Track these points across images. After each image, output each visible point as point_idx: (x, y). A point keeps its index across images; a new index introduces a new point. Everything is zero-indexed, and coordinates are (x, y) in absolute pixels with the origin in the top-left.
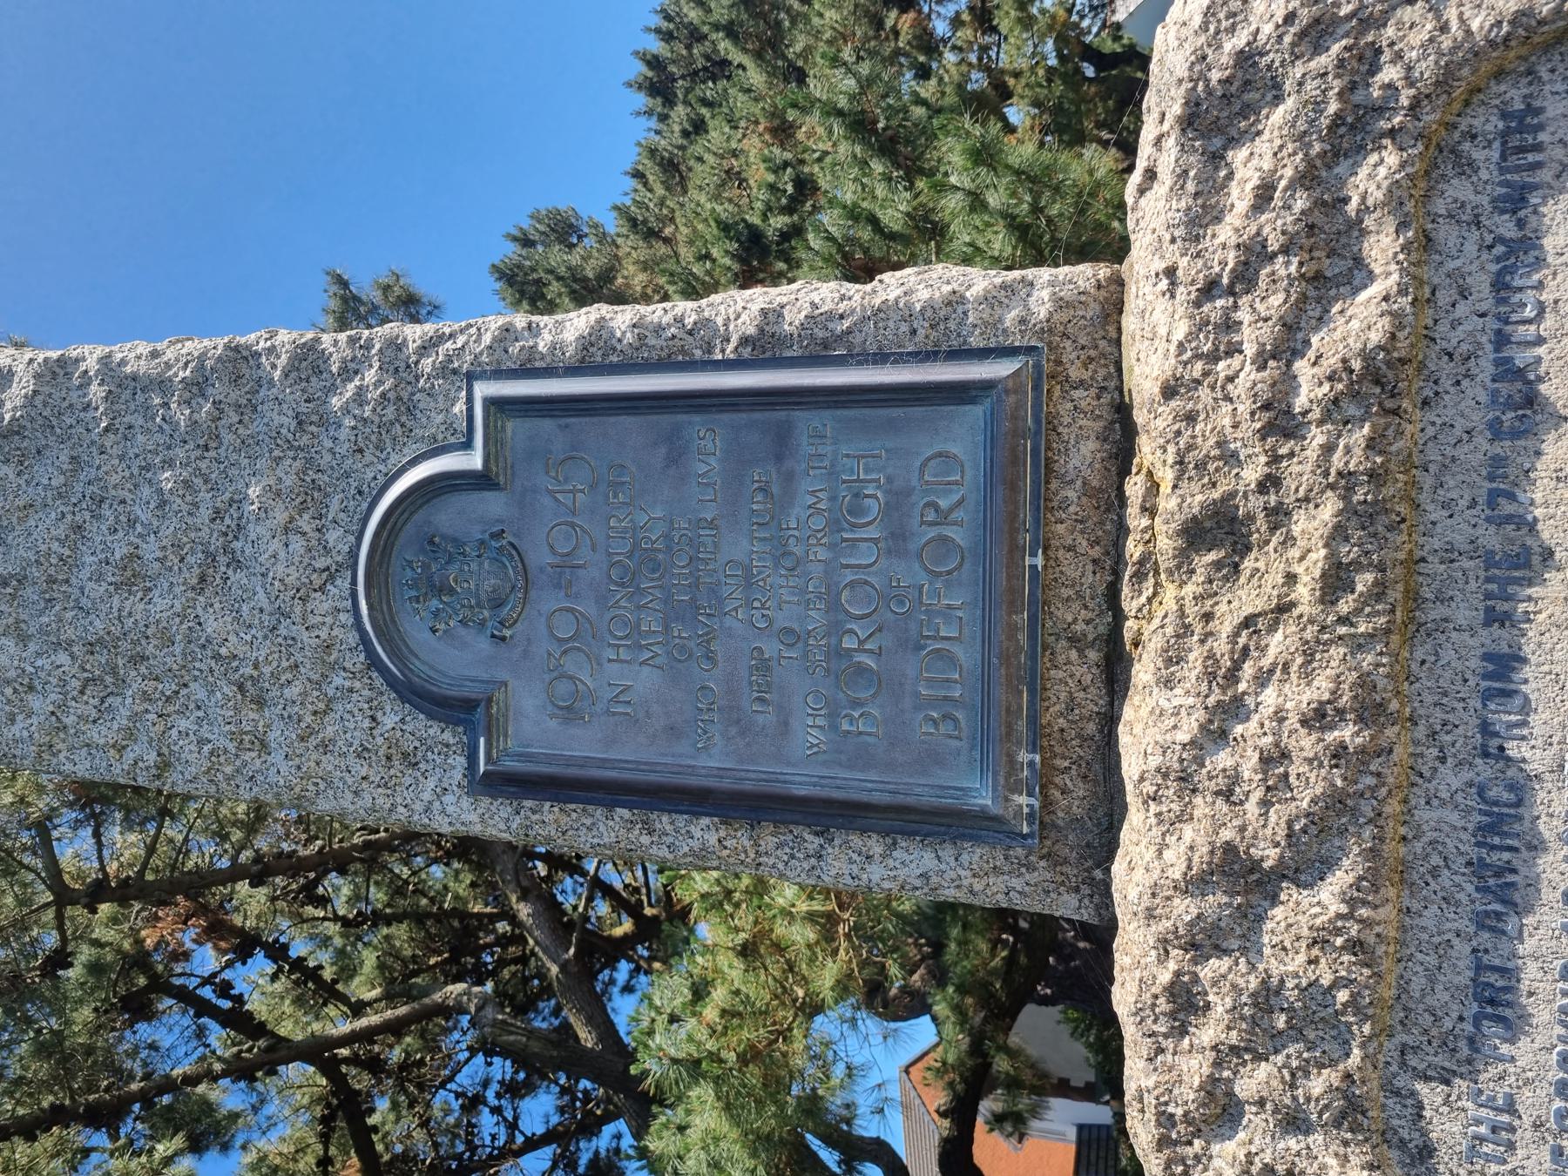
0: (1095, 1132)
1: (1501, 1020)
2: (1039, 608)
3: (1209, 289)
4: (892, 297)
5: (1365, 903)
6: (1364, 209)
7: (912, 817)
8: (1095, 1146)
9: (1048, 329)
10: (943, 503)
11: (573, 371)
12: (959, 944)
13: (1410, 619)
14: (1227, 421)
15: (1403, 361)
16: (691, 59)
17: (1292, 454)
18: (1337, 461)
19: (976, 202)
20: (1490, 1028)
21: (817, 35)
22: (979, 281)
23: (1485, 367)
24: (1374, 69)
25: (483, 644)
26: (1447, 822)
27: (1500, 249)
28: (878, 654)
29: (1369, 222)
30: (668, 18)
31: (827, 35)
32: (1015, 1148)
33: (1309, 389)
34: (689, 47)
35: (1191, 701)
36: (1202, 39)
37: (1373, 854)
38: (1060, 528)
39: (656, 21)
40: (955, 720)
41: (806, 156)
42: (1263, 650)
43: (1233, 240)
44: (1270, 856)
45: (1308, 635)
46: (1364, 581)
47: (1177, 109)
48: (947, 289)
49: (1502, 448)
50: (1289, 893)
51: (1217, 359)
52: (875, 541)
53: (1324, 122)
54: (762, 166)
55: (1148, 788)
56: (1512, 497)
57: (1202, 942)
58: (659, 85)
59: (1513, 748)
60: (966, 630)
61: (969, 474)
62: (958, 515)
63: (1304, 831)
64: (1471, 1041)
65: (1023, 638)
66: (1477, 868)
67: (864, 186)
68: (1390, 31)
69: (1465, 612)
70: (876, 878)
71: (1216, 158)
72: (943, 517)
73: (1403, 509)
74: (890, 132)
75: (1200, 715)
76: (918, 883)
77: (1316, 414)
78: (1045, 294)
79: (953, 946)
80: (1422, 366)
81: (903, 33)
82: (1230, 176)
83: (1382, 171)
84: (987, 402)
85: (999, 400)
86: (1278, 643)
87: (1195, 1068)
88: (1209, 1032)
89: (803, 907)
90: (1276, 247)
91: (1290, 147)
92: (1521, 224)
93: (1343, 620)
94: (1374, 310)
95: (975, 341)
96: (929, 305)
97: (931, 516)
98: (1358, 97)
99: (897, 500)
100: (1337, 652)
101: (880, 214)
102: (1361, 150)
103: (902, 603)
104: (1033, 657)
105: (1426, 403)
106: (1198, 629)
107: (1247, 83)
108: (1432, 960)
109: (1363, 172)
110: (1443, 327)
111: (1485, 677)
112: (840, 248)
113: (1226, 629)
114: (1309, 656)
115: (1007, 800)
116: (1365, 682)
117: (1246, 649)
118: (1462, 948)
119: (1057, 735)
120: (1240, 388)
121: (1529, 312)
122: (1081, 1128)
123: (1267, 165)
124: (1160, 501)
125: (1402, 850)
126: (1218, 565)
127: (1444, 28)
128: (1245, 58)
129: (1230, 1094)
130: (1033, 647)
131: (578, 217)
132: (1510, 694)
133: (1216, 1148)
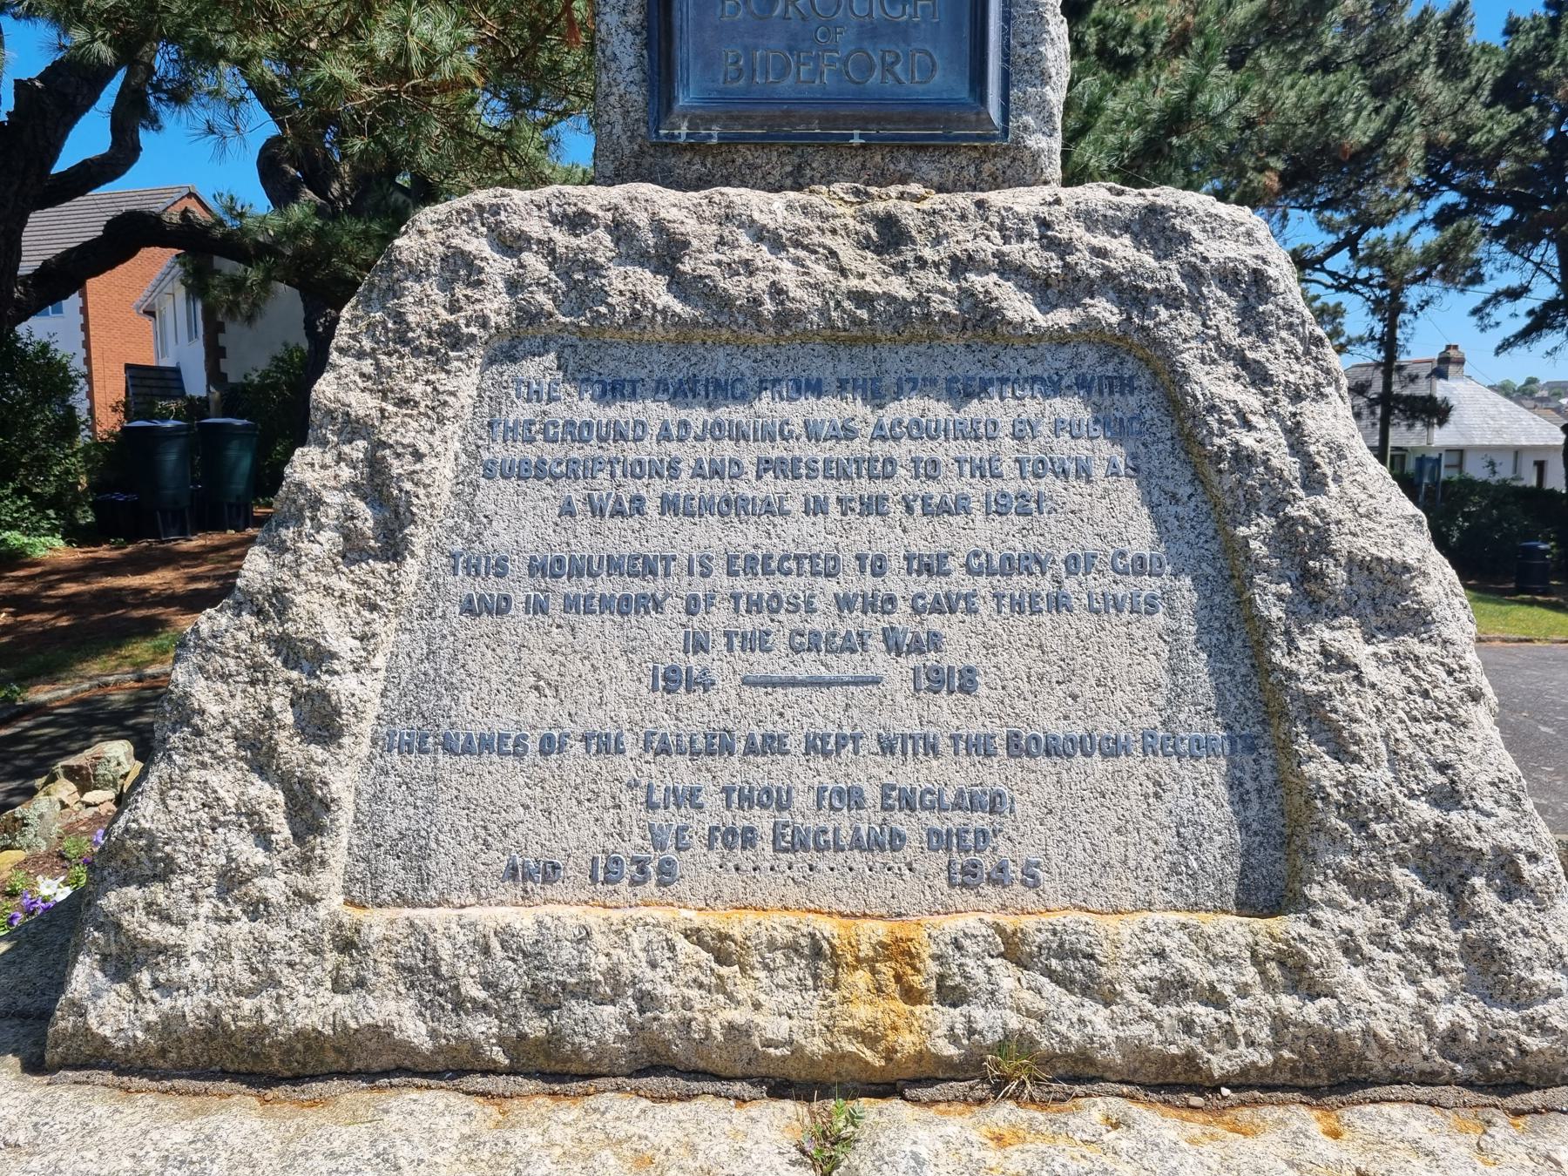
1: (604, 393)
3: (1044, 224)
4: (1050, 28)
5: (665, 319)
6: (1085, 307)
7: (663, 44)
8: (162, 383)
9: (1018, 145)
10: (898, 68)
12: (365, 232)
13: (840, 339)
14: (960, 238)
15: (994, 331)
17: (940, 273)
18: (936, 297)
20: (598, 388)
21: (1274, 83)
22: (1056, 96)
23: (988, 374)
24: (1167, 307)
26: (719, 363)
27: (1056, 378)
28: (784, 17)
29: (1078, 310)
31: (1272, 94)
32: (138, 308)
33: (976, 281)
35: (780, 220)
36: (1201, 213)
37: (695, 323)
38: (878, 158)
40: (738, 78)
41: (1155, 68)
42: (817, 261)
43: (1074, 236)
44: (686, 266)
45: (827, 286)
46: (863, 314)
47: (1159, 201)
48: (1053, 71)
49: (942, 384)
50: (662, 281)
51: (1000, 230)
52: (870, 14)
53: (1140, 283)
54: (1151, 19)
55: (717, 198)
56: (913, 389)
57: (621, 230)
59: (766, 395)
60: (805, 86)
61: (920, 88)
62: (890, 79)
63: (705, 285)
64: (588, 380)
65: (801, 129)
66: (694, 379)
67: (1118, 122)
68: (1188, 314)
69: (844, 370)
70: (607, 18)
71: (1126, 228)
72: (888, 68)
73: (907, 334)
74: (1166, 149)
75: (772, 226)
76: (608, 53)
77: (964, 284)
78: (1044, 145)
79: (360, 227)
80: (990, 343)
81: (1260, 177)
82: (1114, 236)
83: (1107, 315)
84: (970, 101)
85: (972, 108)
86: (821, 271)
87: (535, 227)
88: (561, 238)
89: (413, 43)
90: (1068, 259)
91: (1128, 265)
92: (1069, 387)
93: (838, 304)
94: (1026, 314)
95: (1014, 93)
96: (1042, 58)
97: (889, 59)
98: (1153, 299)
99: (901, 32)
100: (819, 302)
101: (1091, 137)
102: (1120, 303)
103: (824, 36)
104: (788, 136)
105: (968, 346)
106: (826, 226)
107: (1170, 240)
108: (632, 359)
109: (1108, 306)
110: (1012, 353)
111: (807, 380)
113: (828, 240)
114: (815, 286)
115: (684, 116)
116: (801, 316)
117: (816, 252)
118: (643, 374)
119: (730, 157)
120: (982, 242)
121: (1018, 393)
122: (176, 371)
123: (1118, 254)
124: (904, 203)
125: (697, 342)
126: (867, 237)
127: (1185, 341)
128: (1186, 238)
129: (521, 250)
130: (795, 137)
132: (799, 390)
133: (484, 241)
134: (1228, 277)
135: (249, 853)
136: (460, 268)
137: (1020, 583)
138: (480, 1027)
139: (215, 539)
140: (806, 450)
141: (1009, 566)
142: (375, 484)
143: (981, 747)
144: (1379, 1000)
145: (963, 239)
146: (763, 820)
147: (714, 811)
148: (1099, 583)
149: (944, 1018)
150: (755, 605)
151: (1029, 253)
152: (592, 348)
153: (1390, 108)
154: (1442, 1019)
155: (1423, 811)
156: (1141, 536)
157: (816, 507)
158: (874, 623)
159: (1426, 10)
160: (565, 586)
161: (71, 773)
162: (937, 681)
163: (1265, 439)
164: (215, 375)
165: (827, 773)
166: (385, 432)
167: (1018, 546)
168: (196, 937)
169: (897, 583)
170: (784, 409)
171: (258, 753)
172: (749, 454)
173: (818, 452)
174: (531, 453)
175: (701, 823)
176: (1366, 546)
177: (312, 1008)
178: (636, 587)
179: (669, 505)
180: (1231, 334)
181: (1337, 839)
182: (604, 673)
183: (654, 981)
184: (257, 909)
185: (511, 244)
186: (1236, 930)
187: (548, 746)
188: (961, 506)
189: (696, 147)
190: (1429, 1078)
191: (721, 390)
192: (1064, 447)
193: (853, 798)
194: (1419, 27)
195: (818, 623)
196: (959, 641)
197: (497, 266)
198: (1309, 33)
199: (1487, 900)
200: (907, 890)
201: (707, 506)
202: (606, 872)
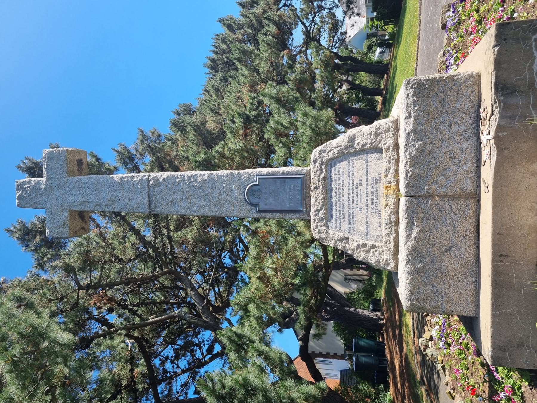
0: (345, 372)
2: (305, 194)
11: (266, 175)
16: (223, 59)
19: (304, 124)
25: (258, 199)
26: (329, 206)
30: (216, 47)
34: (222, 55)
39: (213, 48)
57: (316, 215)
58: (214, 67)
86: (319, 195)
87: (315, 224)
88: (316, 222)
89: (271, 266)
99: (294, 186)
112: (274, 130)
131: (192, 106)
134: (320, 154)
135: (377, 252)
136: (319, 232)
137: (351, 175)
138: (393, 229)
139: (387, 351)
140: (338, 197)
141: (349, 176)
142: (341, 240)
143: (367, 179)
144: (390, 142)
145: (316, 181)
146: (375, 201)
147: (374, 206)
148: (351, 167)
149: (392, 184)
150: (353, 202)
151: (318, 174)
152: (328, 217)
153: (267, 22)
154: (392, 135)
155: (372, 136)
156: (346, 163)
157: (343, 196)
158: (355, 190)
159: (241, 15)
160: (351, 221)
161: (425, 350)
162: (361, 183)
163: (336, 151)
164: (342, 357)
165: (370, 194)
166: (336, 239)
167: (347, 175)
168: (385, 257)
169: (351, 187)
170: (333, 199)
171: (368, 252)
172: (338, 202)
173: (338, 195)
174: (338, 225)
175: (375, 208)
176: (347, 141)
177: (392, 246)
178: (351, 214)
179: (343, 211)
180: (326, 154)
181: (375, 145)
182: (360, 217)
183: (389, 212)
184: (383, 251)
185: (317, 227)
186: (384, 154)
187: (367, 223)
188: (343, 181)
189: (306, 208)
190: (397, 136)
191: (332, 205)
192: (337, 170)
193: (372, 192)
194: (245, 16)
195: (355, 195)
196: (357, 181)
197: (319, 228)
198: (251, 53)
199: (380, 131)
200: (382, 187)
201: (343, 207)
202: (380, 217)
